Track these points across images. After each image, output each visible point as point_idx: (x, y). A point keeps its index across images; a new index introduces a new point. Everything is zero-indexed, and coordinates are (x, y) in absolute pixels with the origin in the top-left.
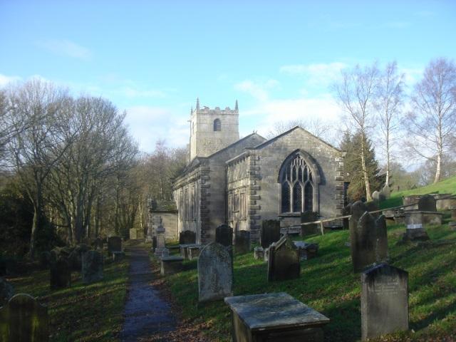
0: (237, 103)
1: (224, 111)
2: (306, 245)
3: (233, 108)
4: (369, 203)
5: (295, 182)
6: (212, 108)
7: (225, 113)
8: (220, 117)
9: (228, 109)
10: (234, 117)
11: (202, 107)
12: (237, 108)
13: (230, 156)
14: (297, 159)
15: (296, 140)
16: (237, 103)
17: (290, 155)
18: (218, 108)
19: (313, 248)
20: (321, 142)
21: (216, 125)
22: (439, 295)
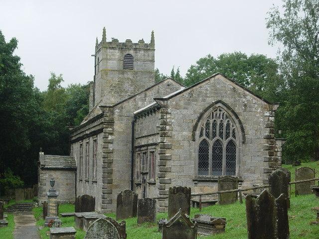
0: (153, 33)
1: (136, 44)
2: (212, 219)
3: (148, 41)
4: (38, 156)
5: (229, 139)
6: (122, 40)
7: (138, 47)
8: (132, 52)
9: (142, 41)
10: (150, 53)
11: (109, 40)
12: (153, 41)
13: (140, 103)
14: (218, 112)
15: (216, 90)
16: (153, 33)
17: (210, 107)
18: (129, 41)
19: (219, 224)
20: (247, 93)
21: (128, 62)
22: (137, 174)
